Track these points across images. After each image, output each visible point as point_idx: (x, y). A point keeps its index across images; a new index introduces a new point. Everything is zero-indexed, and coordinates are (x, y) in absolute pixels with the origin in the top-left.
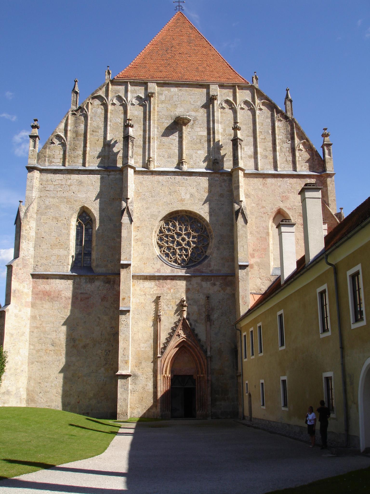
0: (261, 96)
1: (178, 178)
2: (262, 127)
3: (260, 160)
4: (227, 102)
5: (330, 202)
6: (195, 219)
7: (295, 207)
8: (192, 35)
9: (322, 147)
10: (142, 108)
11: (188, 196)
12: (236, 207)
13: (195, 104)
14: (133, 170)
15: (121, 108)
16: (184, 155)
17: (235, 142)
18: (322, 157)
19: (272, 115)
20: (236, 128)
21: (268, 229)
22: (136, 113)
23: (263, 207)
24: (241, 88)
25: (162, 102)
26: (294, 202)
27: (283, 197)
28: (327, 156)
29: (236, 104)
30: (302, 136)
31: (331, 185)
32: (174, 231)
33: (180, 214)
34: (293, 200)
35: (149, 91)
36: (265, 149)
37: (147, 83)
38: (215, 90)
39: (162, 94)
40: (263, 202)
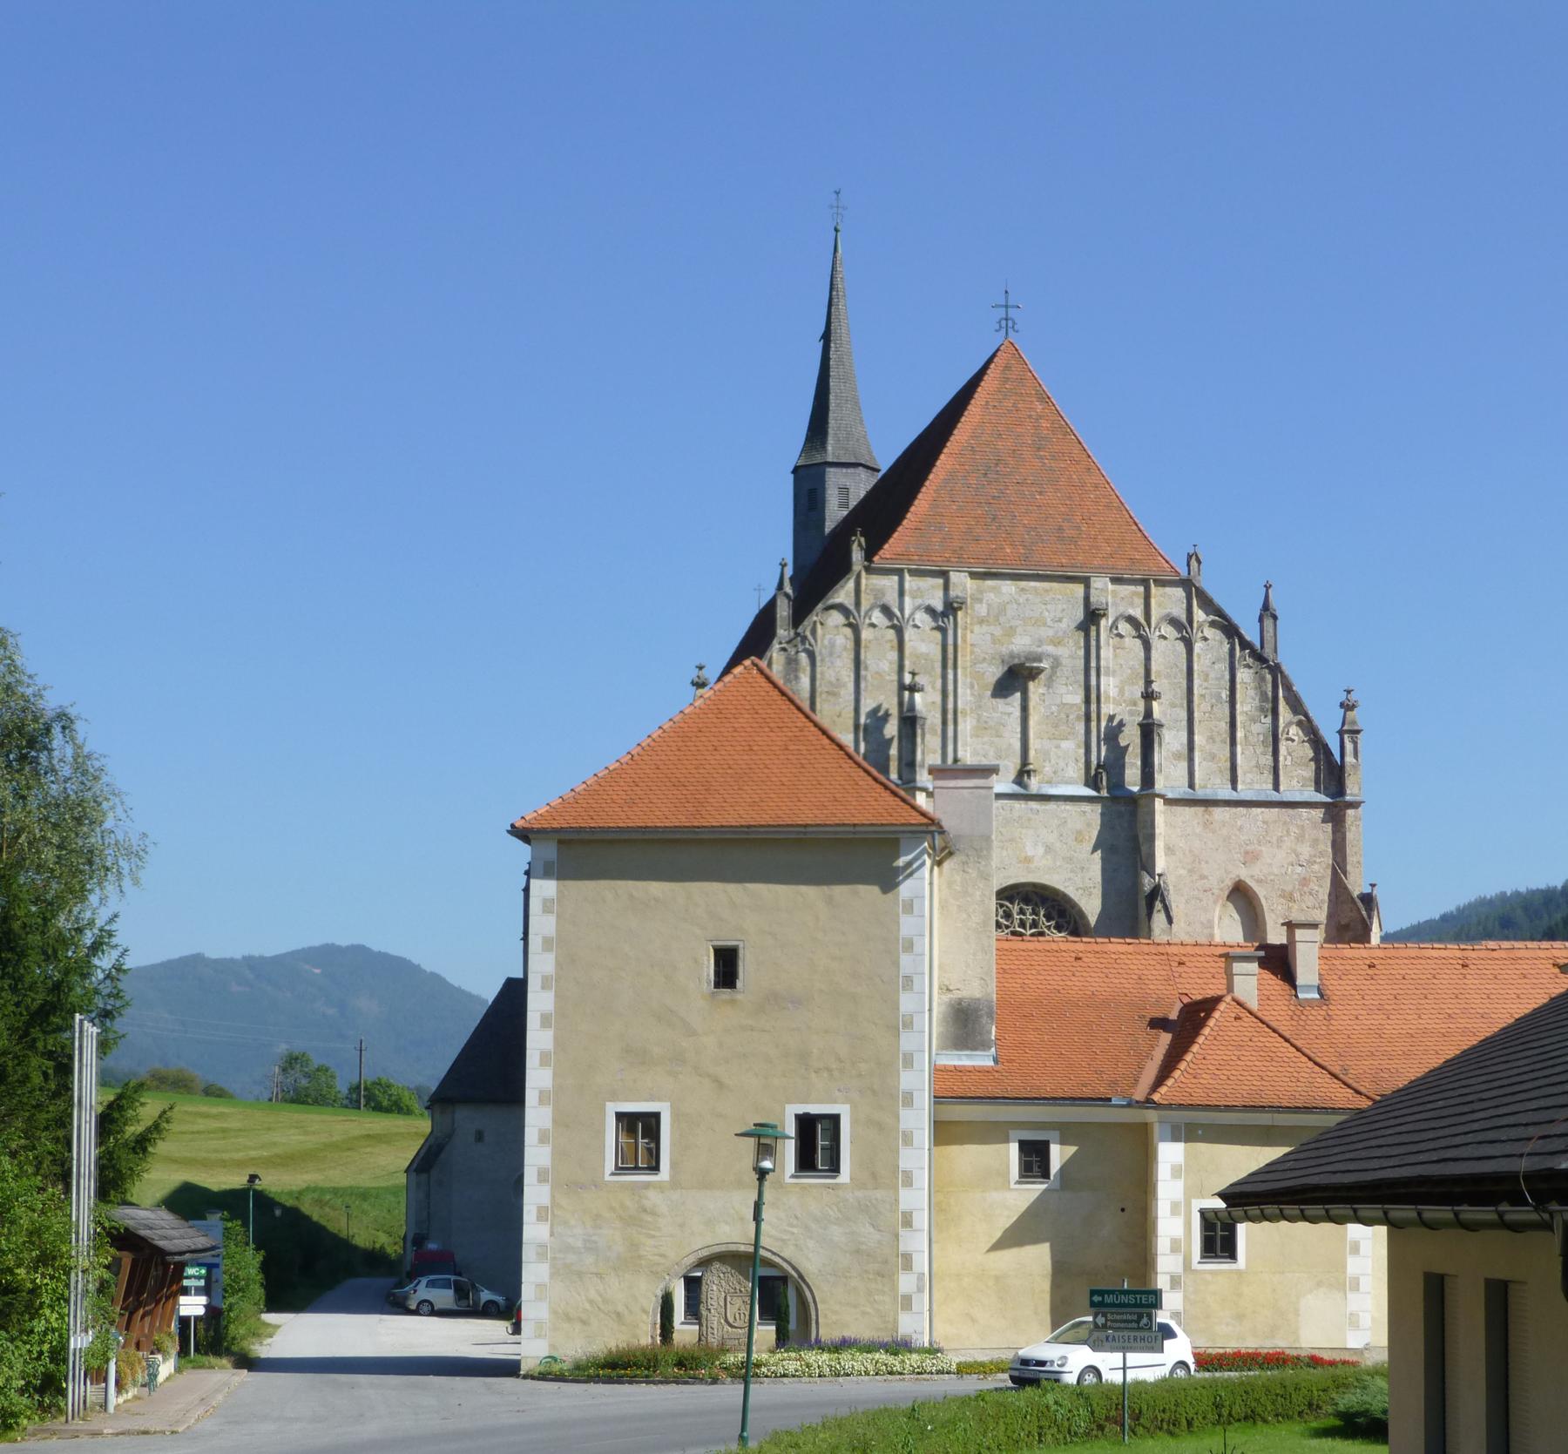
0: (1208, 604)
1: (1019, 806)
2: (1205, 684)
3: (1200, 763)
4: (1131, 620)
5: (1349, 868)
6: (1054, 900)
7: (1272, 877)
8: (1044, 424)
9: (1341, 733)
10: (938, 635)
11: (1041, 850)
12: (1147, 883)
13: (1056, 625)
14: (924, 794)
15: (891, 634)
16: (1032, 753)
17: (1148, 731)
18: (1342, 1118)
19: (1232, 651)
20: (1149, 696)
21: (1212, 927)
22: (923, 648)
23: (1203, 877)
24: (1161, 583)
25: (981, 621)
26: (1270, 865)
27: (1247, 853)
28: (1349, 759)
29: (1150, 628)
30: (1296, 705)
31: (1353, 828)
32: (1007, 927)
33: (1021, 889)
34: (1269, 861)
35: (952, 593)
36: (1211, 739)
37: (948, 572)
38: (1103, 590)
39: (980, 601)
40: (1204, 865)
